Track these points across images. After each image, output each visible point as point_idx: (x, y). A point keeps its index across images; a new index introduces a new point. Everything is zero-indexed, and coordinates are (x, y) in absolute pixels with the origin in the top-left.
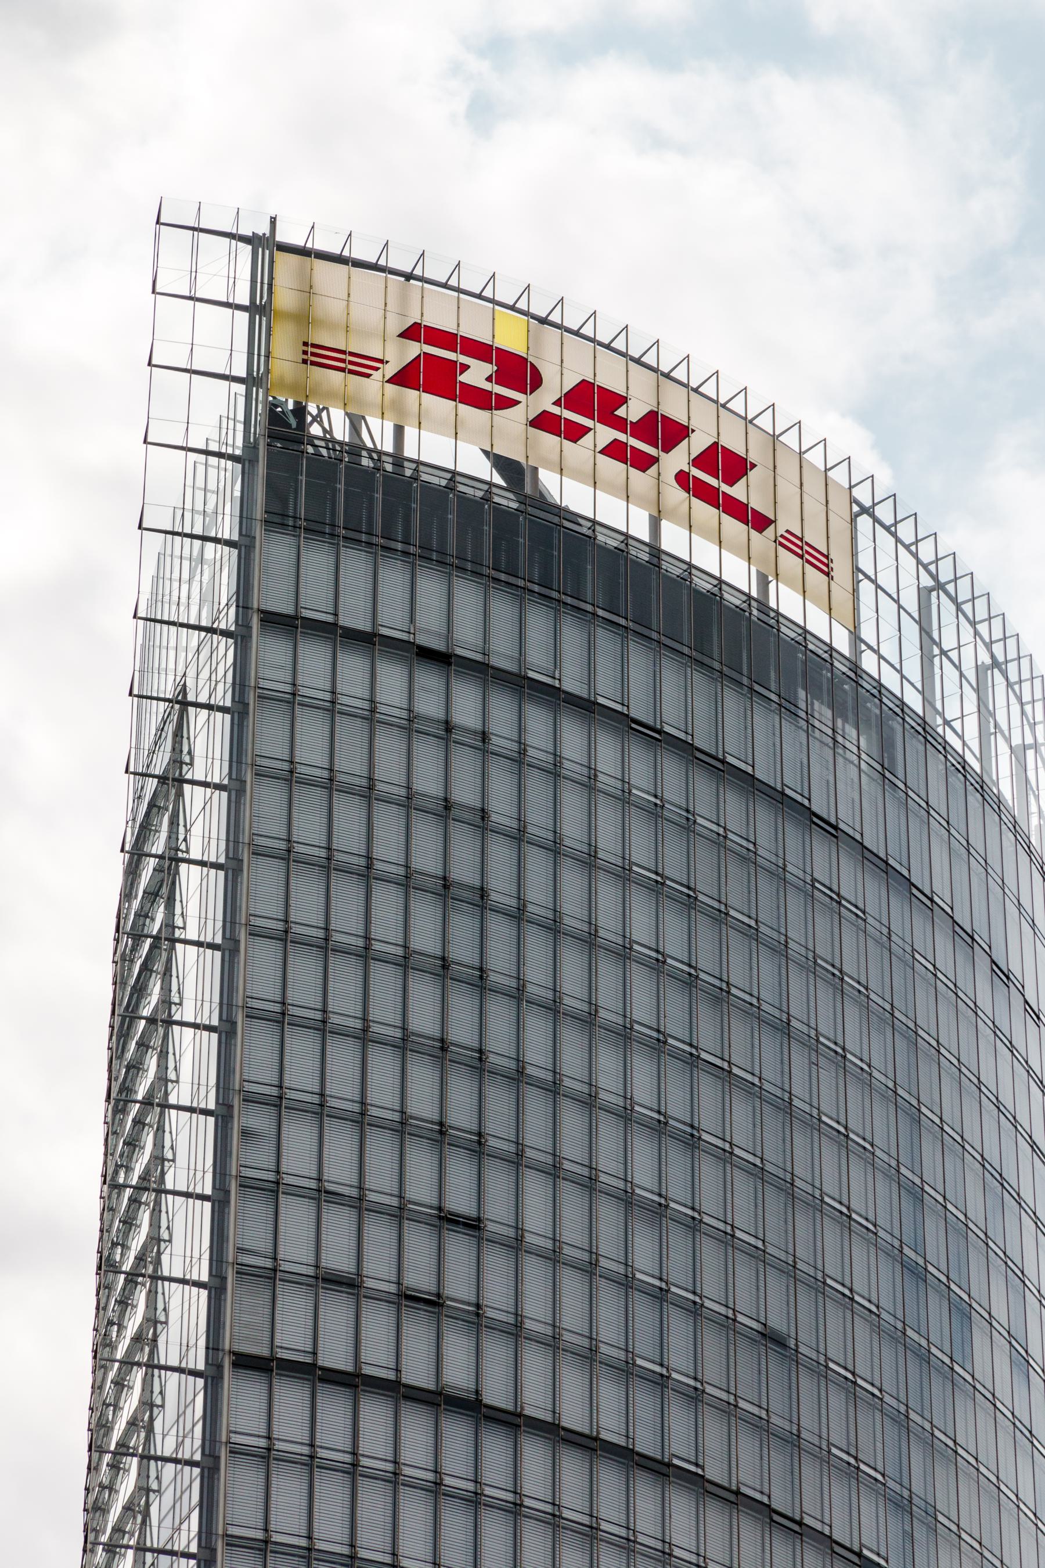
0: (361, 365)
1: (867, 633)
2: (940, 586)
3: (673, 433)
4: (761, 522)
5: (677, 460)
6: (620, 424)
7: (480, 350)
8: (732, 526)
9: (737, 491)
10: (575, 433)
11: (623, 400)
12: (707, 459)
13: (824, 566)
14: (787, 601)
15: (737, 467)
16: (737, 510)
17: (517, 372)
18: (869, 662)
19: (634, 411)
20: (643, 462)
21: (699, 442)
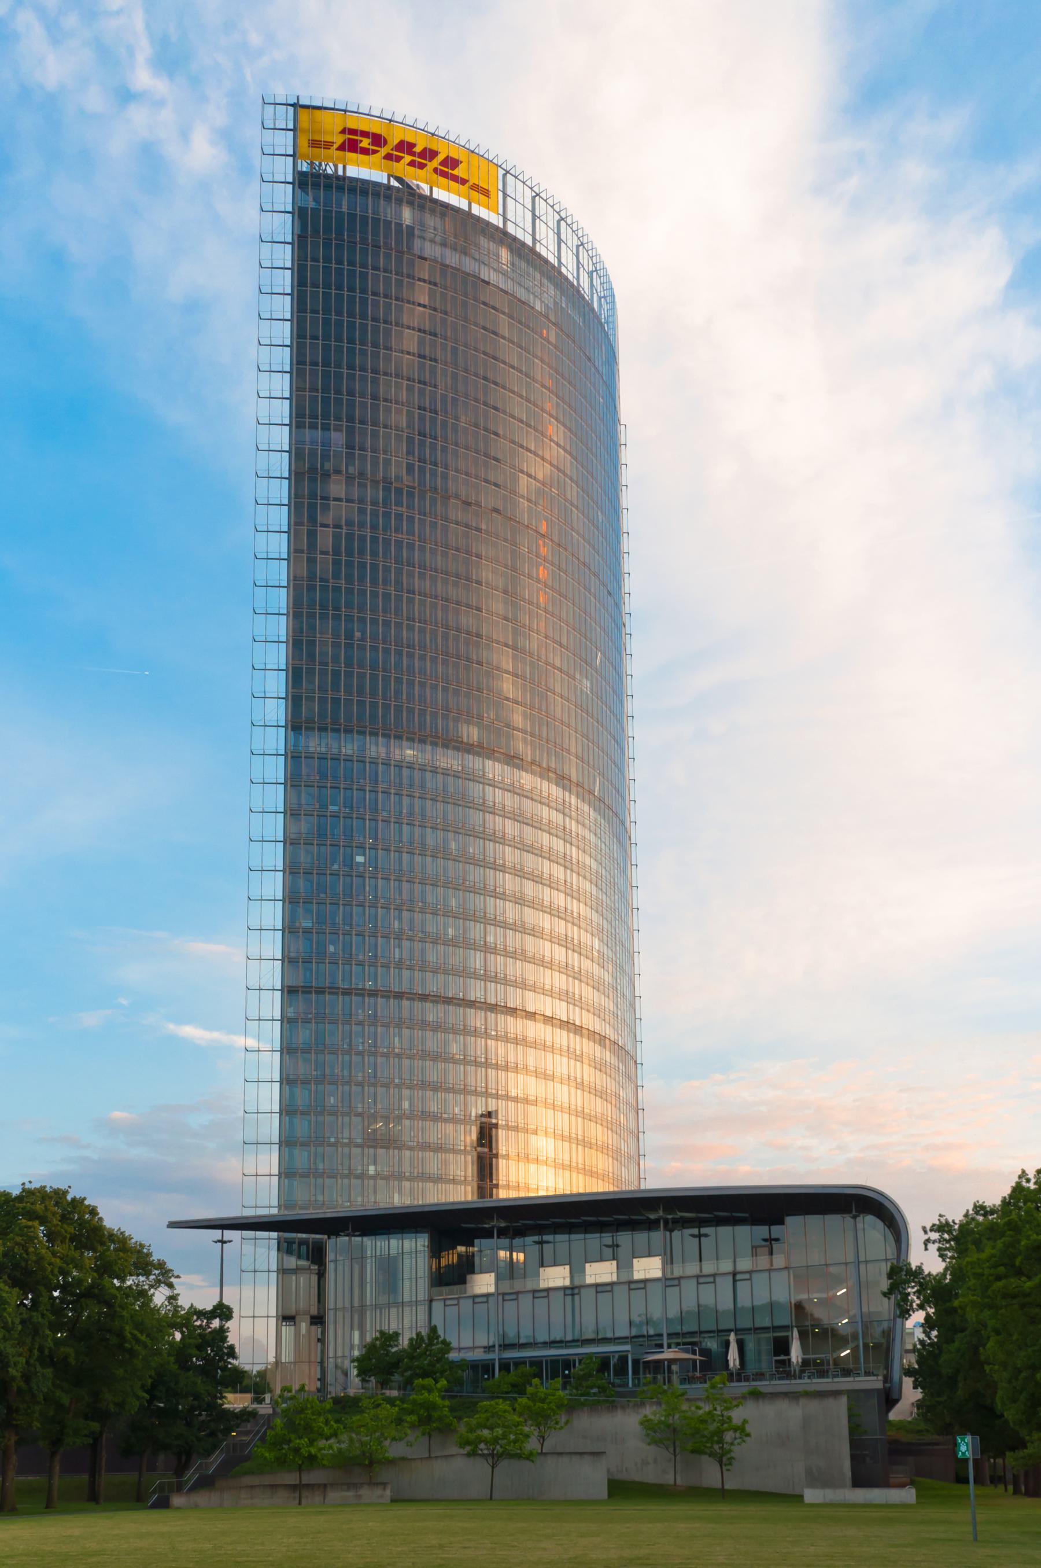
0: (328, 145)
1: (563, 260)
2: (582, 244)
3: (432, 154)
4: (464, 182)
5: (435, 163)
6: (413, 154)
7: (365, 134)
8: (453, 184)
9: (455, 172)
10: (399, 159)
11: (414, 145)
12: (444, 163)
13: (486, 193)
14: (476, 210)
15: (455, 163)
16: (455, 179)
17: (378, 140)
18: (564, 270)
19: (418, 149)
20: (422, 166)
21: (441, 157)
